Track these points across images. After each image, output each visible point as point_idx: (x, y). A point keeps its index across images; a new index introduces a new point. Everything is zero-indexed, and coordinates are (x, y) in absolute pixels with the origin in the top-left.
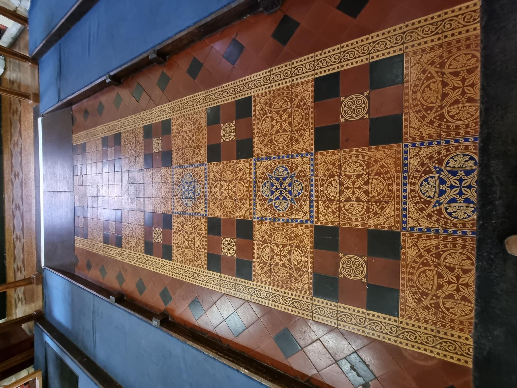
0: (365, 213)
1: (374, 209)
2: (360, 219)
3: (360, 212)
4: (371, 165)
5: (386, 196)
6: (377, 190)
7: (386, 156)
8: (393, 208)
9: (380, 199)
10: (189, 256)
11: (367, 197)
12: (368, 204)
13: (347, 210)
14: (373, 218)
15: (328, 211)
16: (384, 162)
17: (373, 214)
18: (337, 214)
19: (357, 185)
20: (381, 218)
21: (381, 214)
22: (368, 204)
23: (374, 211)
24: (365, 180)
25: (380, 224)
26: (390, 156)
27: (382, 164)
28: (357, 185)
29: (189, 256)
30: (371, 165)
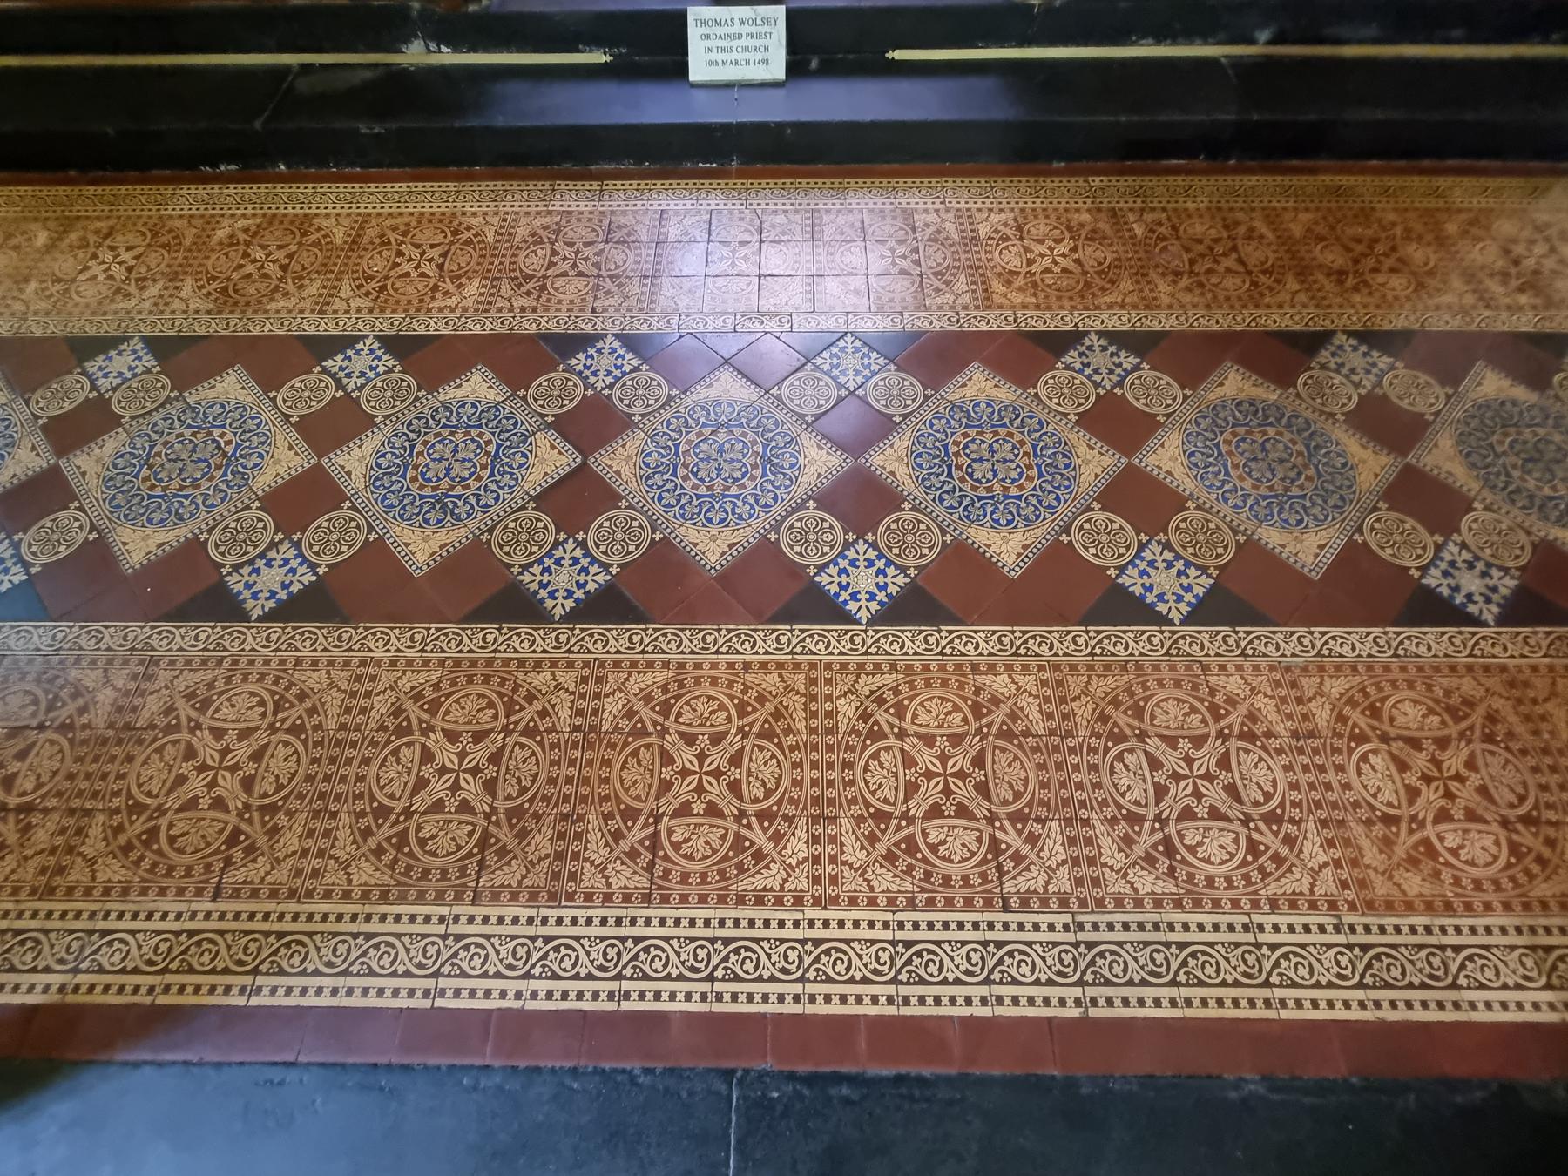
0: (872, 810)
1: (888, 834)
2: (604, 790)
3: (627, 790)
4: (766, 824)
5: (929, 868)
6: (689, 839)
7: (1049, 867)
8: (632, 884)
9: (158, 842)
10: (467, 258)
11: (920, 814)
12: (901, 818)
13: (635, 753)
14: (605, 831)
15: (634, 700)
16: (773, 861)
17: (872, 833)
18: (625, 725)
19: (691, 782)
20: (351, 848)
21: (874, 855)
22: (901, 818)
23: (625, 832)
24: (721, 804)
25: (843, 852)
26: (1050, 878)
27: (1026, 857)
28: (691, 782)
29: (467, 258)
30: (766, 824)
